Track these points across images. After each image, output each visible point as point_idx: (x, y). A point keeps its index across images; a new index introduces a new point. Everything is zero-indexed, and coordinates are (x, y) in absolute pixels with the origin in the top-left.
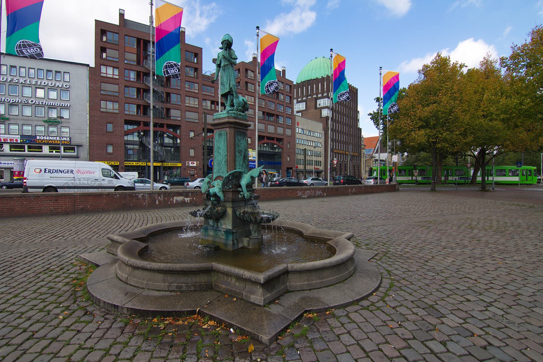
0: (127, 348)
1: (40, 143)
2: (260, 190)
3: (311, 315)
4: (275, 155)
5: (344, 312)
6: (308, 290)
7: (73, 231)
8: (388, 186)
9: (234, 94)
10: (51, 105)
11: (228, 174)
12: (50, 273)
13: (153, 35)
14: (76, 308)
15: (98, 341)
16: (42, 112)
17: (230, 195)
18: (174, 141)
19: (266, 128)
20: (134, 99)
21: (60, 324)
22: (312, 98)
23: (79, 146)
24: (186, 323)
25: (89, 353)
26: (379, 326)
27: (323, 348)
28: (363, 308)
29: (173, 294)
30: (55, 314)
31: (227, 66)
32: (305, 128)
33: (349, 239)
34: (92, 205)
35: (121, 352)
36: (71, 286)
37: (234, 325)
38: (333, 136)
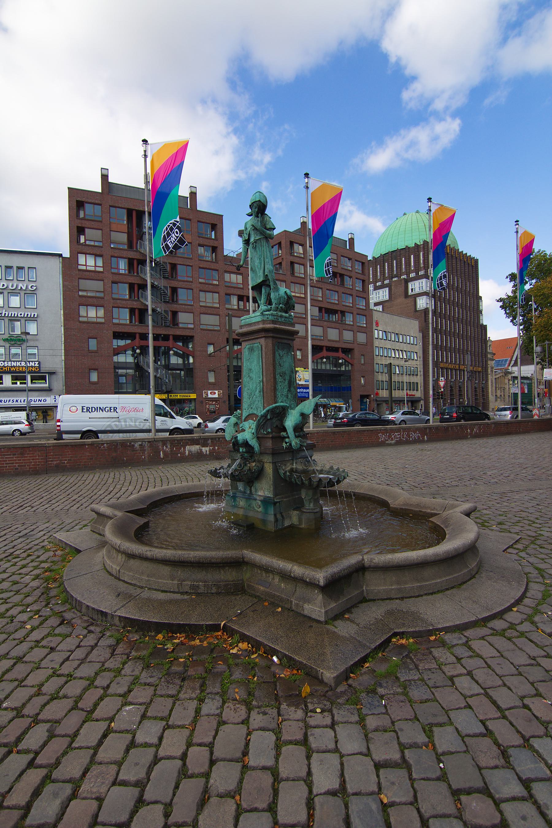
0: (119, 678)
2: (317, 433)
3: (403, 641)
5: (460, 638)
6: (399, 598)
7: (45, 498)
10: (13, 316)
12: (13, 560)
14: (48, 614)
15: (79, 665)
17: (269, 444)
18: (184, 361)
19: (325, 333)
20: (126, 300)
21: (28, 637)
23: (51, 373)
24: (205, 644)
25: (66, 683)
26: (524, 665)
27: (425, 697)
28: (495, 633)
29: (186, 597)
30: (21, 622)
31: (259, 242)
32: (389, 329)
33: (468, 514)
34: (71, 460)
35: (110, 683)
36: (42, 581)
38: (437, 340)
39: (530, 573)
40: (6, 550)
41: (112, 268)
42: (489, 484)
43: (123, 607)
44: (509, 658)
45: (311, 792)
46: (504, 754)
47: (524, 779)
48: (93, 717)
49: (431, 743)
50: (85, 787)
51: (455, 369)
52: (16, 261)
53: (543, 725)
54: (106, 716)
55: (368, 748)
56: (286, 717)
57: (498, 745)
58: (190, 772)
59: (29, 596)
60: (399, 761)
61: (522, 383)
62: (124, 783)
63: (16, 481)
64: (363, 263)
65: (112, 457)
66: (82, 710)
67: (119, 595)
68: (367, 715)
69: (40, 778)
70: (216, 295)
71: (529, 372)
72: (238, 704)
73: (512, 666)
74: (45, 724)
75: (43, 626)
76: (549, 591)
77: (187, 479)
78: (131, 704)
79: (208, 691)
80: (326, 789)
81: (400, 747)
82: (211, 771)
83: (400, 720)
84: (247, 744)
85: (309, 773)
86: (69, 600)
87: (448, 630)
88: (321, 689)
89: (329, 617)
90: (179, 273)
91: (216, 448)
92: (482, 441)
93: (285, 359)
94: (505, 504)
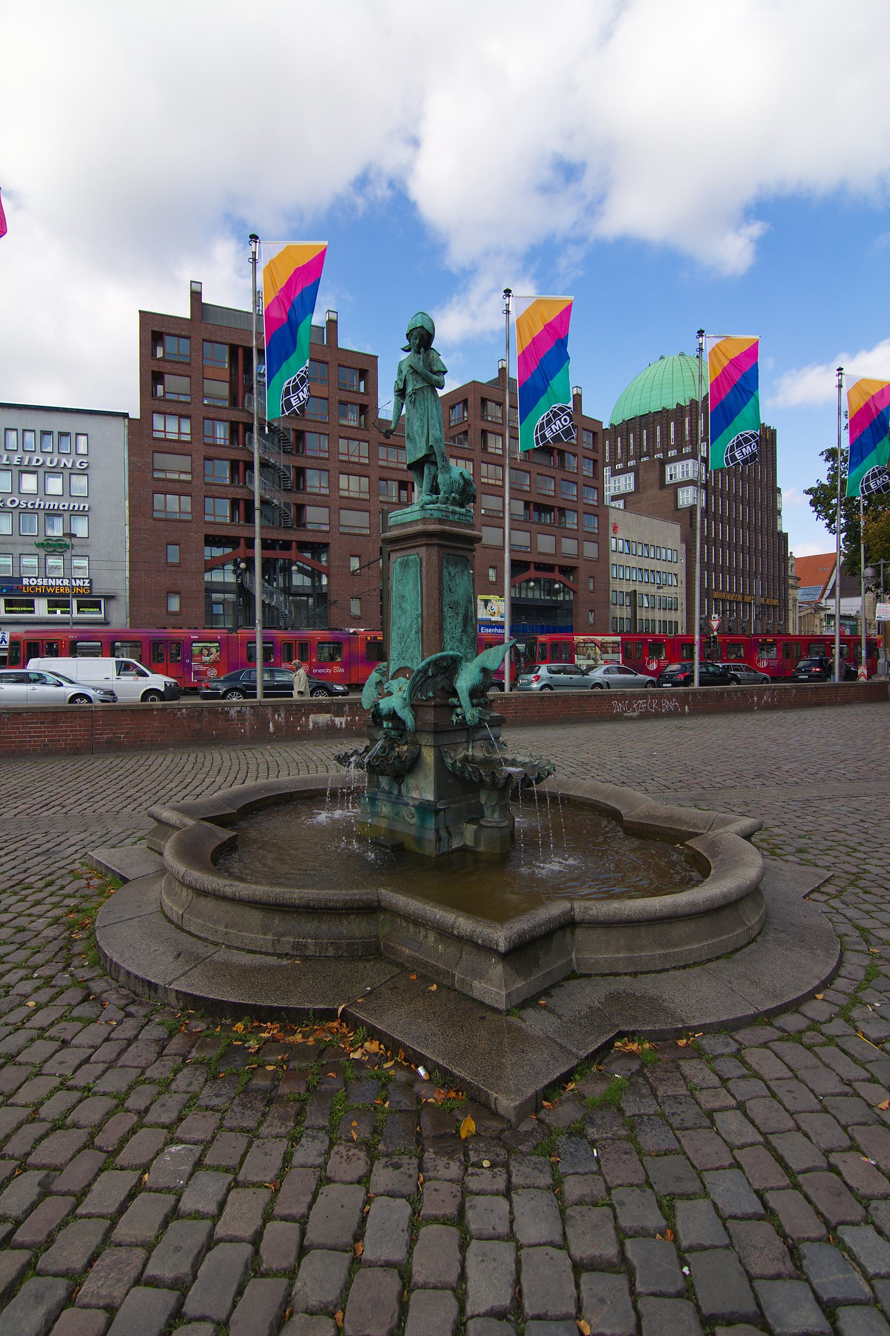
0: (167, 1096)
1: (29, 594)
2: (516, 698)
3: (634, 1047)
4: (557, 608)
5: (727, 1045)
6: (630, 974)
7: (85, 792)
8: (864, 685)
9: (439, 460)
10: (51, 507)
11: (424, 663)
12: (23, 893)
13: (259, 334)
14: (66, 983)
15: (104, 1072)
16: (33, 527)
17: (430, 716)
18: (313, 582)
19: (533, 541)
20: (225, 486)
21: (28, 1020)
22: (652, 462)
23: (109, 598)
24: (311, 1041)
25: (80, 1101)
26: (832, 1095)
27: (664, 1146)
28: (787, 1036)
29: (285, 962)
30: (21, 995)
31: (420, 392)
32: (633, 537)
33: (748, 837)
34: (130, 733)
35: (151, 1104)
36: (62, 928)
37: (427, 1059)
38: (709, 556)
39: (846, 935)
40: (14, 876)
41: (204, 436)
42: (785, 785)
43: (183, 975)
44: (807, 1081)
45: (462, 1310)
46: (793, 1252)
47: (825, 1298)
48: (116, 1162)
49: (671, 1230)
50: (90, 1287)
51: (737, 602)
52: (57, 424)
53: (861, 1203)
54: (137, 1162)
55: (564, 1235)
56: (431, 1174)
57: (784, 1236)
58: (264, 1266)
59: (39, 952)
60: (615, 1260)
61: (841, 625)
62: (154, 1283)
63: (45, 765)
64: (595, 434)
65: (194, 730)
66: (100, 1149)
67: (179, 956)
68: (566, 1174)
69: (18, 1266)
70: (365, 480)
71: (854, 608)
72: (354, 1148)
73: (812, 1096)
74: (36, 1172)
75: (54, 1003)
76: (877, 966)
77: (308, 766)
78: (181, 1141)
79: (307, 1123)
80: (489, 1307)
81: (617, 1235)
82: (299, 1265)
83: (620, 1185)
84: (364, 1220)
85: (463, 1277)
86: (101, 961)
87: (708, 1029)
88: (496, 1125)
89: (514, 1004)
90: (309, 445)
91: (357, 718)
92: (775, 716)
93: (458, 580)
94: (810, 818)
